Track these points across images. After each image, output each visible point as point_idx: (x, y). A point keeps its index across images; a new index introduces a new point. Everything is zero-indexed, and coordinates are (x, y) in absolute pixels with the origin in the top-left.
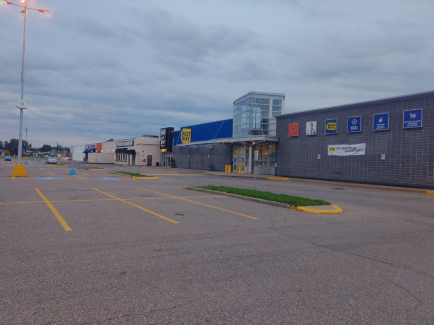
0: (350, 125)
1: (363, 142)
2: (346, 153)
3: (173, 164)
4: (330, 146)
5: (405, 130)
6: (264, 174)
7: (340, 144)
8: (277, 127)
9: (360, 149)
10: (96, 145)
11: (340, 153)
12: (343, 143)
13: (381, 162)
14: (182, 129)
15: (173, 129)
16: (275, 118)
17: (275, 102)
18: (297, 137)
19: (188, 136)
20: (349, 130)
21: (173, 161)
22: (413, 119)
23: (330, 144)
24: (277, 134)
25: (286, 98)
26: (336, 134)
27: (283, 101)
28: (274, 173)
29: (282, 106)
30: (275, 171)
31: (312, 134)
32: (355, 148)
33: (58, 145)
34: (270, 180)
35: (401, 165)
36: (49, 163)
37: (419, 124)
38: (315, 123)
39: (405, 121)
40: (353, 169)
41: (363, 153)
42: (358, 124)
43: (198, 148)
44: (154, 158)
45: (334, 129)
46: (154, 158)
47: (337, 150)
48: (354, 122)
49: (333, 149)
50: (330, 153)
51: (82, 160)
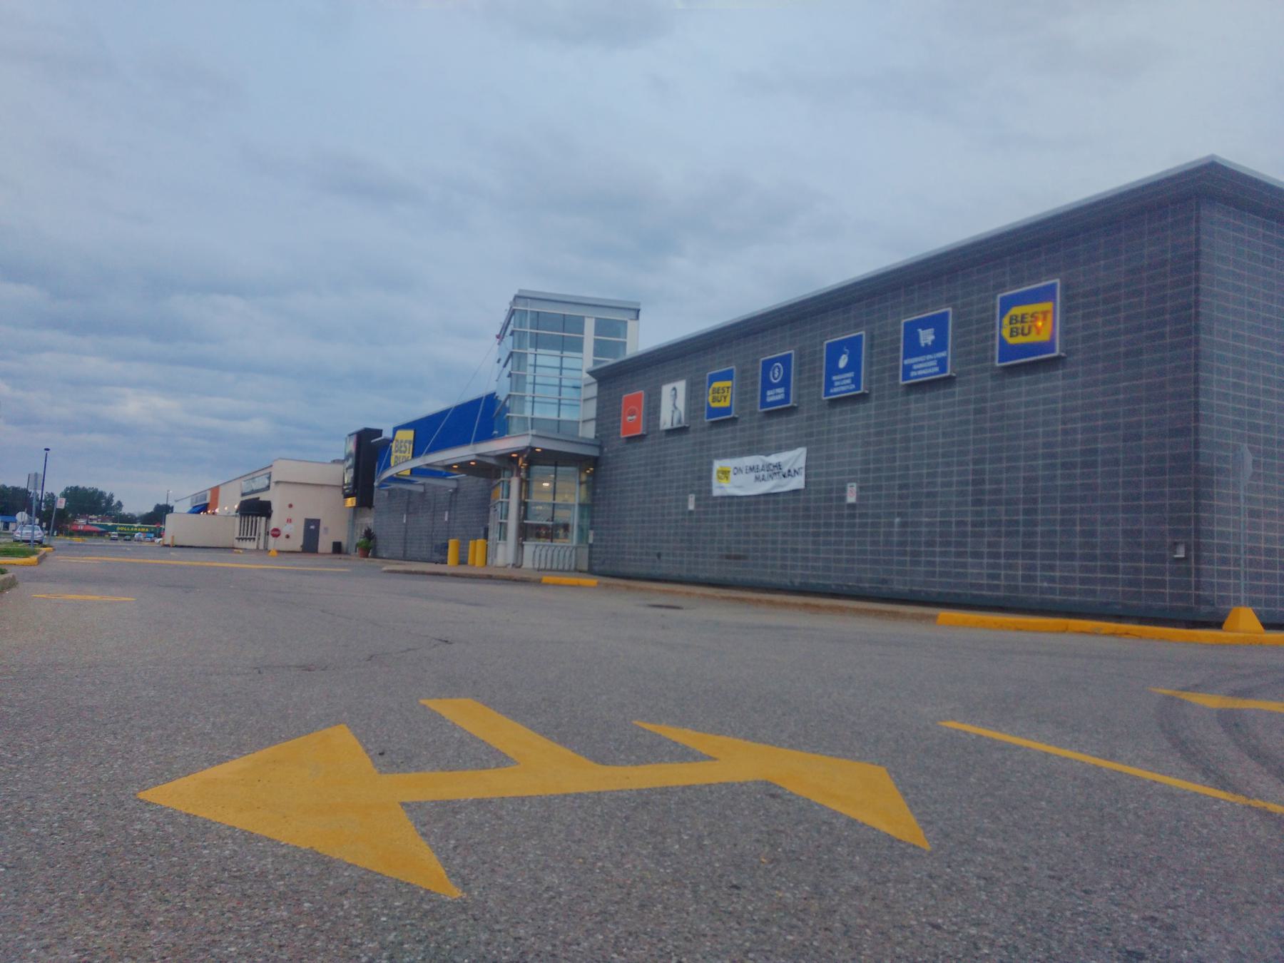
2: (758, 483)
3: (369, 546)
4: (718, 465)
5: (912, 388)
7: (742, 454)
11: (739, 487)
13: (846, 512)
14: (395, 430)
15: (378, 433)
16: (593, 380)
18: (641, 437)
20: (764, 403)
23: (718, 457)
24: (597, 431)
26: (734, 420)
28: (585, 567)
30: (590, 558)
31: (675, 426)
32: (778, 466)
34: (547, 584)
35: (897, 520)
37: (942, 364)
38: (681, 386)
39: (905, 358)
40: (1083, 533)
41: (798, 482)
43: (418, 488)
44: (326, 529)
45: (727, 404)
46: (326, 529)
47: (736, 477)
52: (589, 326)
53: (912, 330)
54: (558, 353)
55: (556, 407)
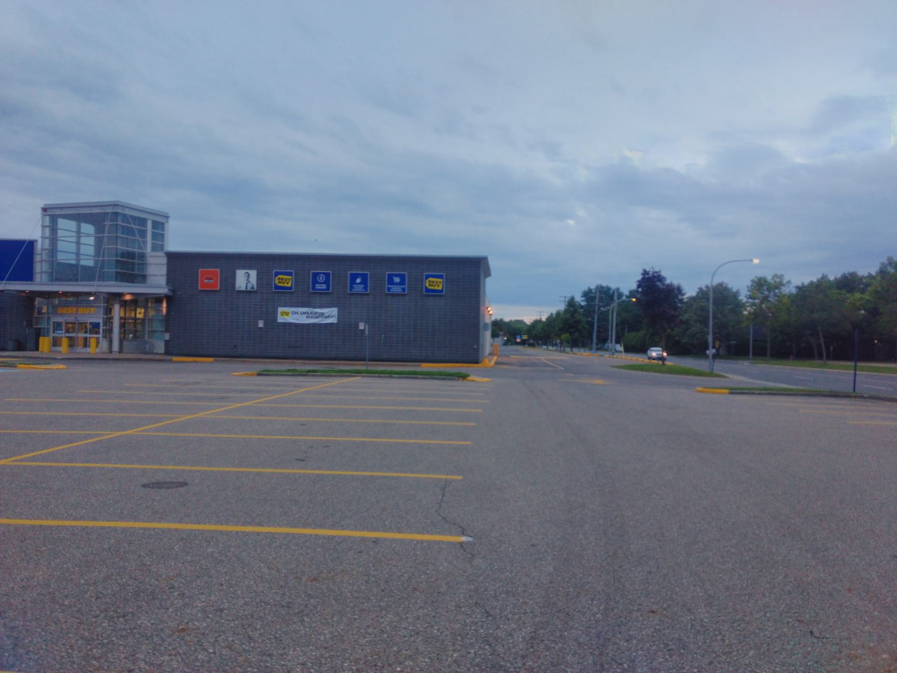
0: (315, 282)
1: (334, 306)
4: (280, 309)
5: (351, 294)
6: (341, 360)
8: (168, 271)
9: (330, 315)
12: (302, 306)
17: (156, 225)
20: (314, 288)
22: (397, 284)
23: (280, 306)
25: (170, 220)
27: (181, 239)
29: (165, 232)
31: (249, 289)
32: (323, 314)
33: (645, 273)
34: (176, 362)
37: (404, 289)
41: (334, 320)
42: (327, 282)
47: (291, 315)
48: (321, 278)
49: (287, 314)
50: (281, 319)
52: (149, 224)
53: (390, 277)
54: (853, 364)
55: (81, 252)
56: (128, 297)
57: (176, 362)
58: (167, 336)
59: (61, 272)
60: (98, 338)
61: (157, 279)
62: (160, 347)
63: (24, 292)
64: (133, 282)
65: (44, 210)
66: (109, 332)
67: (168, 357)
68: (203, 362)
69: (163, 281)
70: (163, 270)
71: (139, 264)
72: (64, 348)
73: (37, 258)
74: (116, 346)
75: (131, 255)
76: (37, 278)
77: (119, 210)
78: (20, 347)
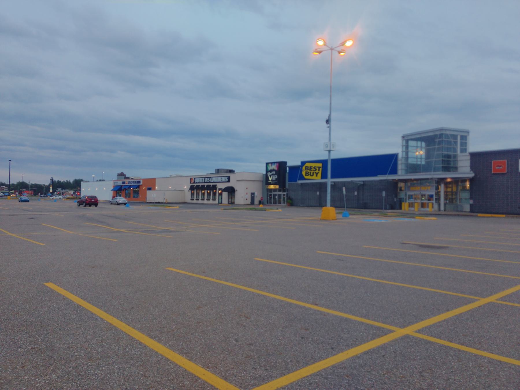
8: (471, 163)
10: (142, 181)
19: (317, 171)
21: (289, 198)
25: (470, 133)
27: (476, 145)
34: (480, 217)
36: (119, 204)
51: (249, 201)
52: (459, 138)
56: (449, 180)
57: (480, 217)
58: (471, 202)
59: (413, 168)
60: (433, 203)
61: (464, 169)
62: (467, 208)
63: (395, 180)
64: (449, 171)
65: (403, 137)
66: (438, 200)
67: (472, 214)
68: (498, 217)
69: (468, 169)
70: (468, 163)
71: (453, 161)
72: (416, 208)
73: (399, 162)
74: (442, 208)
75: (449, 156)
76: (399, 172)
77: (444, 132)
78: (392, 208)
